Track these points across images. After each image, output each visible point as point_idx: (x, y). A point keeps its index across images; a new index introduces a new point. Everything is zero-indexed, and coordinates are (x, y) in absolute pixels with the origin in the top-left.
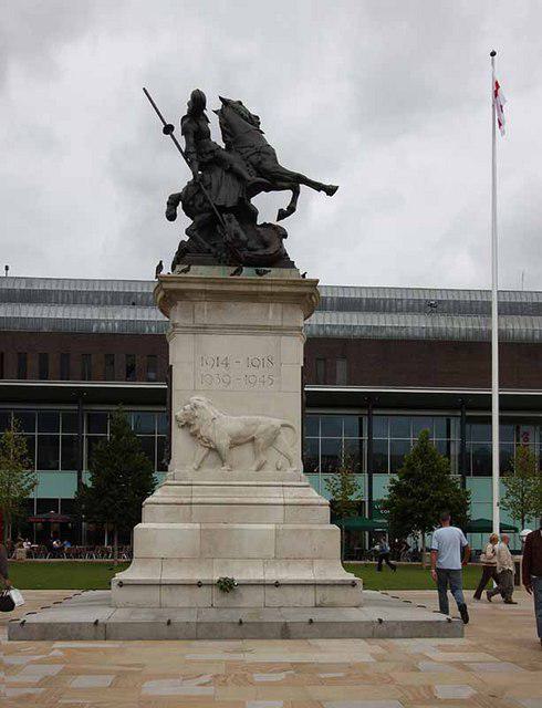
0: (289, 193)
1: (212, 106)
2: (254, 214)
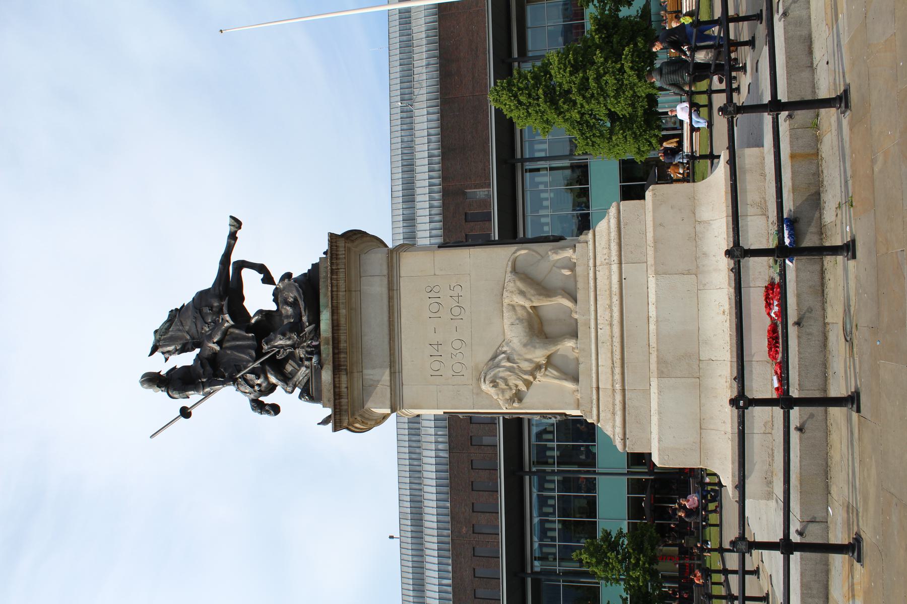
0: (246, 273)
1: (161, 365)
2: (265, 315)
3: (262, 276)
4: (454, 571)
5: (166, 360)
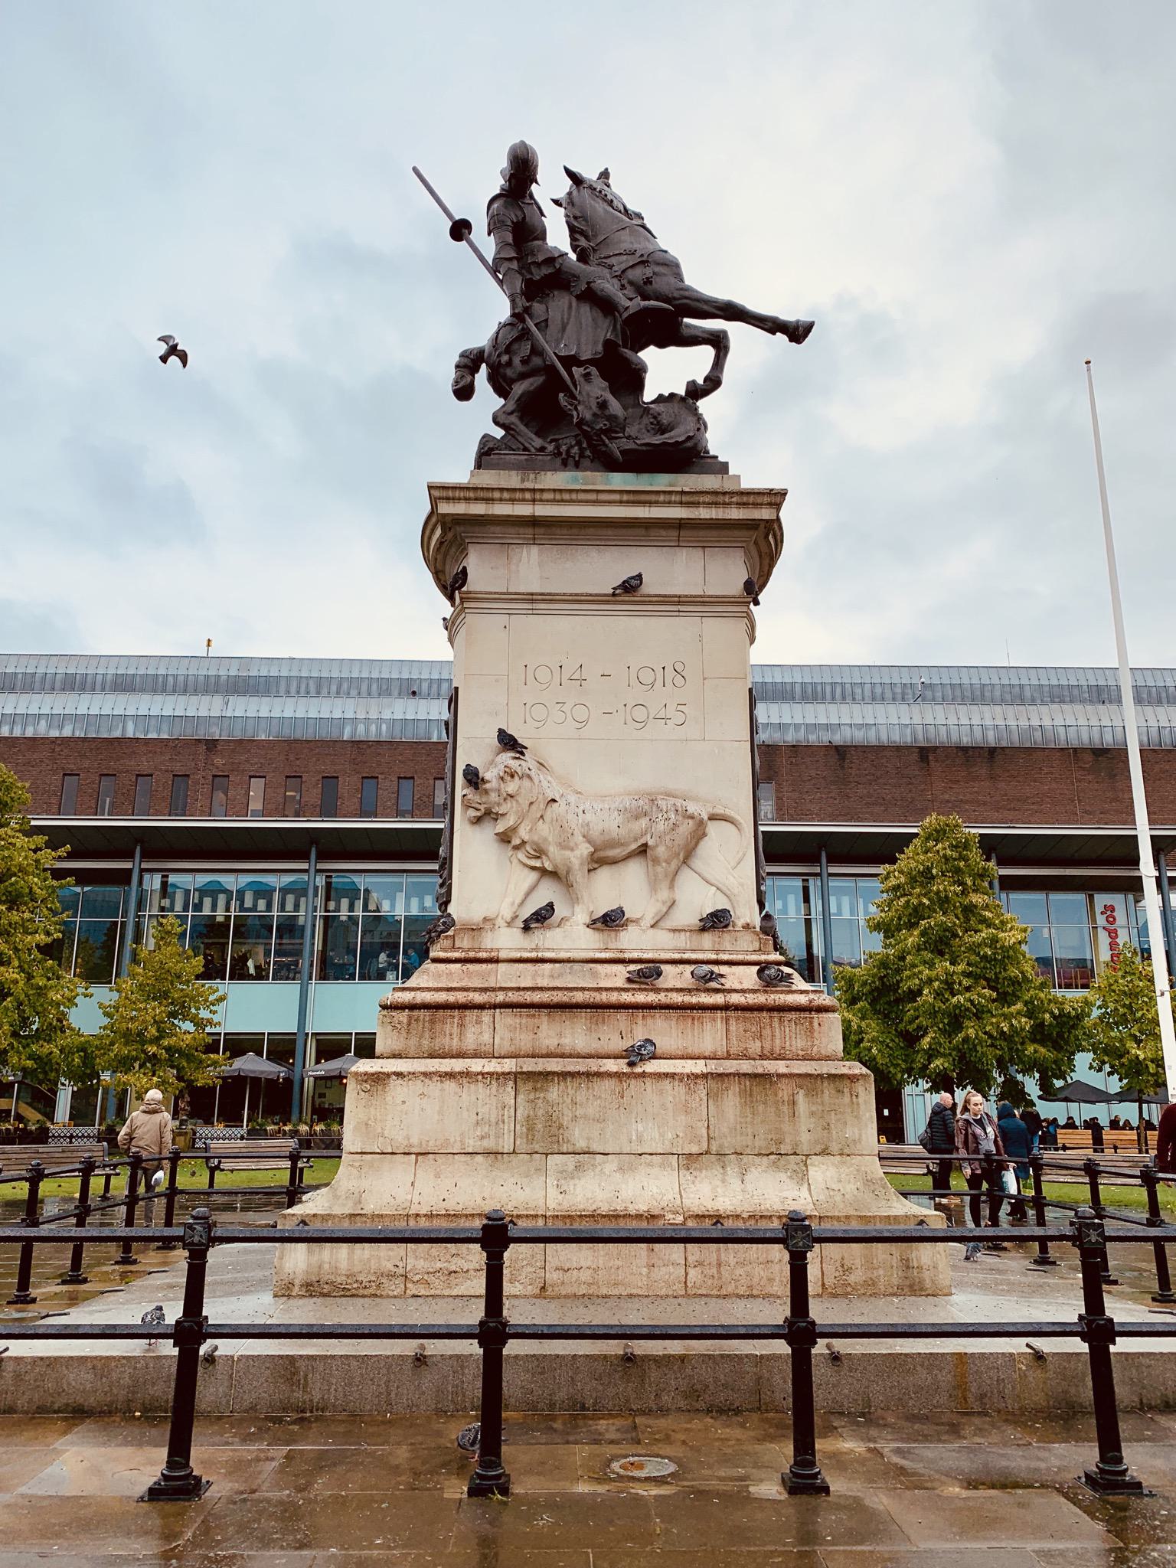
0: (707, 353)
1: (549, 187)
3: (700, 381)
4: (147, 741)
5: (557, 202)
